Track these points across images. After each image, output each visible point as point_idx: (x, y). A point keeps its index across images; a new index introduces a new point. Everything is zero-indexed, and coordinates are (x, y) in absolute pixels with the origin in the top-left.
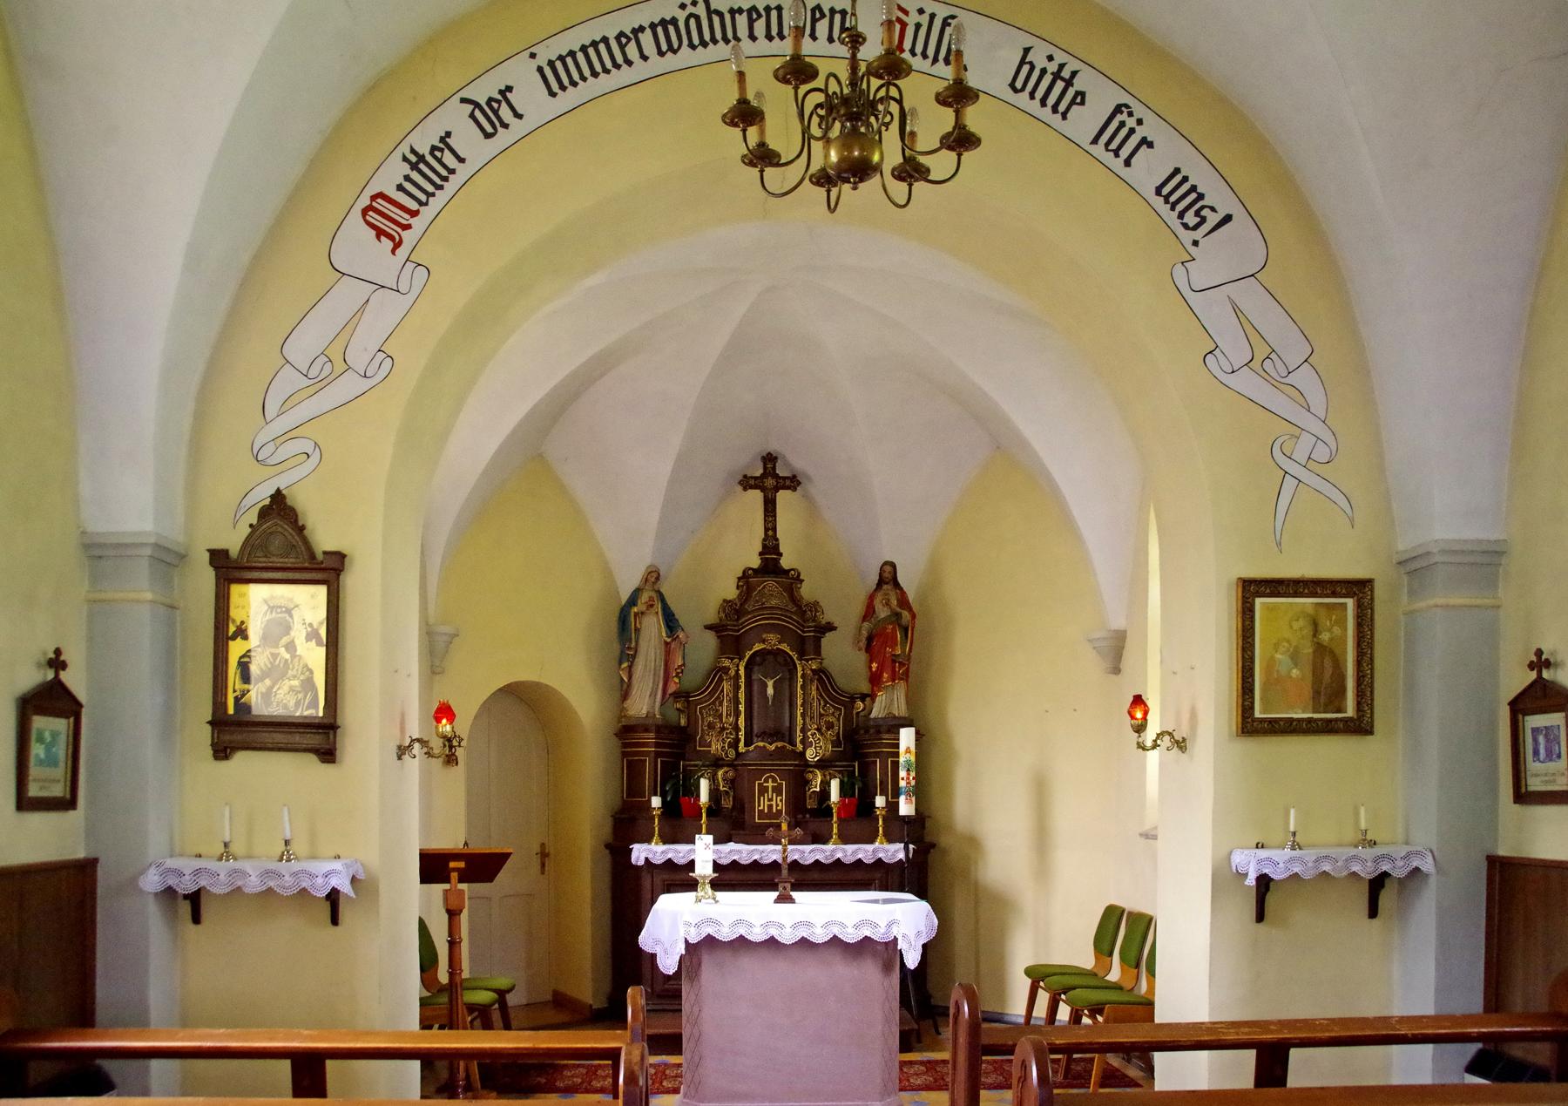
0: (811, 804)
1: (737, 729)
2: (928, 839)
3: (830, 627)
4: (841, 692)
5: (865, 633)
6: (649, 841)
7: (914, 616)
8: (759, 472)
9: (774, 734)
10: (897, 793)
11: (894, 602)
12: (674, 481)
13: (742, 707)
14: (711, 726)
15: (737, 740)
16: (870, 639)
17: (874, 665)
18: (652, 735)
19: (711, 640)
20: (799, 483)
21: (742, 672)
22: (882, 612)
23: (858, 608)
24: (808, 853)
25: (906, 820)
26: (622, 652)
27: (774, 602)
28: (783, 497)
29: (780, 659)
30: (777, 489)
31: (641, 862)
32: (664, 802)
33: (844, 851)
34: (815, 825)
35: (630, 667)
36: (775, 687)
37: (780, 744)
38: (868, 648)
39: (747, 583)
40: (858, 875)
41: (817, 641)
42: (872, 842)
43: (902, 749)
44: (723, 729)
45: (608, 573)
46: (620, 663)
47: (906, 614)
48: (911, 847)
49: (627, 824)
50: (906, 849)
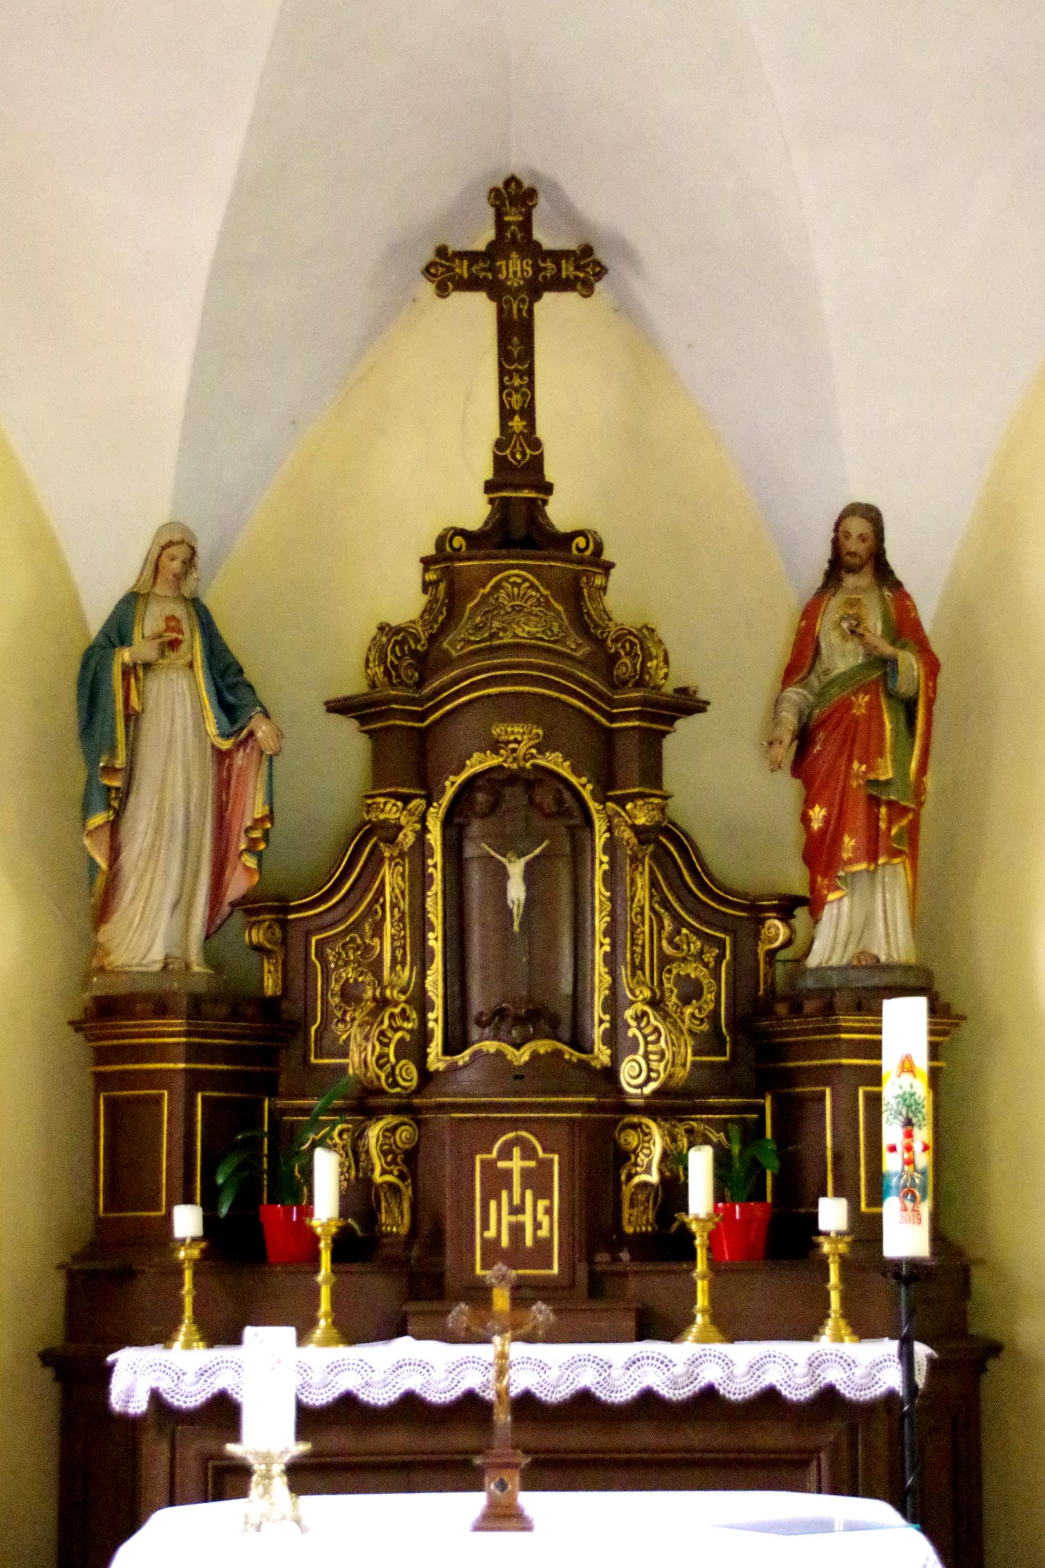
0: (636, 1220)
1: (423, 1004)
2: (976, 1328)
3: (687, 704)
4: (724, 894)
5: (790, 720)
6: (163, 1337)
7: (932, 666)
8: (482, 237)
9: (529, 1017)
10: (878, 1193)
11: (875, 624)
12: (230, 267)
13: (435, 941)
14: (349, 995)
15: (423, 1036)
16: (804, 737)
17: (818, 814)
18: (178, 1024)
19: (348, 745)
20: (601, 272)
21: (435, 837)
22: (841, 656)
23: (776, 645)
24: (621, 1369)
25: (910, 1273)
26: (90, 781)
27: (524, 631)
28: (554, 314)
29: (545, 798)
30: (535, 290)
31: (139, 1405)
32: (209, 1221)
33: (728, 1363)
34: (648, 1285)
35: (114, 827)
36: (530, 876)
37: (544, 1046)
38: (800, 766)
39: (449, 576)
40: (772, 1437)
41: (652, 744)
42: (808, 1332)
43: (889, 1062)
44: (382, 1003)
45: (43, 547)
46: (87, 810)
47: (909, 663)
48: (922, 1351)
49: (107, 1290)
50: (907, 1357)
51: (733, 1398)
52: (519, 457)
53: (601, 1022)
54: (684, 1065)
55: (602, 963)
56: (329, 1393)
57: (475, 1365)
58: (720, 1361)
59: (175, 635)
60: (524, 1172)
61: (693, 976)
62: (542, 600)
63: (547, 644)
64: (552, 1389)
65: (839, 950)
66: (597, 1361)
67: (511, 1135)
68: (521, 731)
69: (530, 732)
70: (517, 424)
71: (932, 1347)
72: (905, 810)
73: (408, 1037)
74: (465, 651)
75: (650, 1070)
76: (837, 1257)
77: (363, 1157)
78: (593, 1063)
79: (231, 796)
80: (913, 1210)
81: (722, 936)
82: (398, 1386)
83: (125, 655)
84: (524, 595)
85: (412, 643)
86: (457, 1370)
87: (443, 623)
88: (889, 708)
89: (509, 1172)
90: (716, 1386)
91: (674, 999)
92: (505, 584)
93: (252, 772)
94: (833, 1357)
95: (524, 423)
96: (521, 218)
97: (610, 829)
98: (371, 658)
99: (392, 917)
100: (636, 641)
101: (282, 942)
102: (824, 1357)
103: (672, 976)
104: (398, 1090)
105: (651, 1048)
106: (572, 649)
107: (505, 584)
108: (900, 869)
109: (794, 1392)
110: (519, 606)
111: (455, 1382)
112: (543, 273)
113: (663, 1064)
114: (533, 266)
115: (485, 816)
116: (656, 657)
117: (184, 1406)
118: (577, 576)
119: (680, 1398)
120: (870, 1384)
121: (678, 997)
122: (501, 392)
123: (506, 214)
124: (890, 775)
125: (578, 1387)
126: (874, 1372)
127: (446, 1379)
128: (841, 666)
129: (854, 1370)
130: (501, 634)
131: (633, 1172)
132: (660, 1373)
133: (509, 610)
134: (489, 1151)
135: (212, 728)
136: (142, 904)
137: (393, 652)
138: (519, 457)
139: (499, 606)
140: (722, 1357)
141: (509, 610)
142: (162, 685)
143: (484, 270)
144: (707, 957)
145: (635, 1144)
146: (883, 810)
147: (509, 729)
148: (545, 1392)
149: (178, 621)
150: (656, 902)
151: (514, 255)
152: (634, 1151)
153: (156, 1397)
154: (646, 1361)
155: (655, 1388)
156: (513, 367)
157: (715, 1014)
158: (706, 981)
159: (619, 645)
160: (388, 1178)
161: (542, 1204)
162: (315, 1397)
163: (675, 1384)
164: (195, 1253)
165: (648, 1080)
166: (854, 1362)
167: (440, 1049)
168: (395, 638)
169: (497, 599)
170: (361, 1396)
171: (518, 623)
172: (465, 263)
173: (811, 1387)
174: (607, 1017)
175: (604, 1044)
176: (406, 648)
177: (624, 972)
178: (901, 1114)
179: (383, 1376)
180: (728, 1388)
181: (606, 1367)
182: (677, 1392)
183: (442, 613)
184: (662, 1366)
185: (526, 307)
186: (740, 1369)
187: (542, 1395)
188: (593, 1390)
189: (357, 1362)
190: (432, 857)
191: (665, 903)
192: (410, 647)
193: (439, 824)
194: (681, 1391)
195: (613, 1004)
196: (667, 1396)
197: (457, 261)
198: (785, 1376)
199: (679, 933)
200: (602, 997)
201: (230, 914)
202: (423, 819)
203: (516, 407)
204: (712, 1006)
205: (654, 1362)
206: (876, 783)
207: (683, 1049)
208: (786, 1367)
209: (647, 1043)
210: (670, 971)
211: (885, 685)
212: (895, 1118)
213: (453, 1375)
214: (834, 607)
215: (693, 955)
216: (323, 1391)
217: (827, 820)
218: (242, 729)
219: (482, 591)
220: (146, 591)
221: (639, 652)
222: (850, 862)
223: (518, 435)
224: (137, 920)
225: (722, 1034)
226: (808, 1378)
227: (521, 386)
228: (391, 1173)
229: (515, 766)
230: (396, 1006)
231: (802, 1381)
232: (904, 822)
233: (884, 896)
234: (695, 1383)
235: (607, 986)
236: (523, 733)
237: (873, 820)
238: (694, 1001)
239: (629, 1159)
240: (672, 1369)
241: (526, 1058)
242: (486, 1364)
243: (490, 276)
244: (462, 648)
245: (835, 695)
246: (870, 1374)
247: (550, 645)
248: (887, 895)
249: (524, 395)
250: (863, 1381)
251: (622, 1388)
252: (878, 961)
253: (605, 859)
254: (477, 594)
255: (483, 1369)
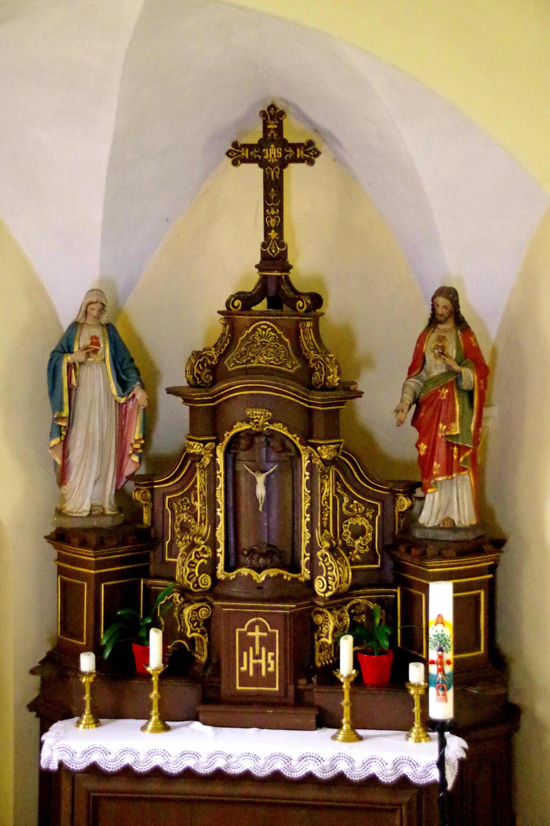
1: (214, 545)
11: (452, 351)
12: (116, 167)
13: (220, 513)
15: (214, 560)
20: (318, 153)
21: (220, 460)
22: (435, 367)
28: (295, 175)
31: (54, 766)
32: (99, 663)
36: (267, 484)
45: (36, 290)
47: (469, 376)
51: (354, 779)
52: (274, 251)
53: (305, 557)
54: (347, 582)
55: (306, 527)
56: (148, 766)
57: (222, 755)
58: (347, 760)
59: (95, 347)
60: (261, 638)
61: (360, 524)
62: (277, 337)
63: (275, 367)
64: (261, 770)
65: (433, 518)
66: (284, 756)
67: (254, 619)
68: (260, 413)
69: (265, 414)
70: (273, 234)
71: (469, 745)
72: (468, 449)
73: (206, 562)
74: (234, 368)
75: (328, 585)
76: (418, 696)
77: (182, 622)
78: (300, 579)
79: (126, 424)
80: (443, 695)
81: (377, 503)
82: (183, 764)
83: (68, 359)
84: (268, 335)
85: (209, 361)
86: (213, 757)
87: (227, 347)
88: (459, 396)
89: (254, 638)
90: (345, 773)
91: (349, 537)
92: (258, 329)
93: (135, 415)
94: (406, 761)
95: (277, 234)
96: (276, 127)
97: (310, 459)
98: (188, 370)
99: (200, 498)
100: (323, 365)
101: (151, 500)
102: (402, 761)
103: (348, 526)
104: (200, 590)
105: (329, 573)
106: (289, 368)
107: (258, 329)
108: (467, 477)
109: (385, 778)
110: (264, 342)
111: (212, 763)
112: (287, 156)
113: (334, 583)
114: (282, 153)
115: (245, 450)
116: (332, 373)
117: (76, 769)
118: (298, 322)
119: (327, 778)
120: (426, 776)
121: (351, 536)
122: (265, 217)
123: (268, 124)
124: (458, 432)
125: (275, 769)
126: (428, 769)
127: (207, 762)
128: (435, 372)
129: (417, 768)
130: (252, 361)
131: (320, 636)
132: (316, 765)
133: (259, 344)
134: (243, 627)
135: (114, 392)
136: (79, 481)
137: (198, 367)
138: (274, 251)
139: (254, 342)
140: (349, 758)
141: (259, 344)
142: (89, 370)
143: (257, 154)
144: (368, 514)
145: (321, 622)
146: (455, 449)
147: (254, 412)
148: (257, 771)
149: (97, 338)
150: (339, 489)
151: (272, 146)
152: (321, 625)
153: (61, 764)
154: (309, 758)
155: (314, 772)
156: (271, 205)
157: (372, 545)
158: (368, 527)
159: (315, 364)
160: (194, 634)
161: (270, 654)
162: (141, 767)
163: (324, 770)
164: (91, 679)
165: (328, 590)
166: (417, 764)
167: (222, 567)
168: (199, 360)
169: (254, 338)
170: (164, 768)
171: (261, 355)
172: (247, 150)
173: (395, 775)
174: (308, 554)
175: (306, 568)
176: (205, 365)
177: (318, 533)
178: (436, 645)
179: (175, 759)
180: (351, 774)
181: (289, 760)
182: (325, 774)
183: (226, 342)
184: (318, 761)
185: (278, 173)
186: (357, 765)
187: (256, 773)
188: (282, 771)
189: (162, 751)
190: (219, 470)
191: (345, 489)
192: (207, 363)
193: (222, 454)
194: (327, 774)
195: (312, 548)
196: (320, 776)
197: (243, 149)
198: (381, 769)
199: (352, 503)
200: (306, 544)
201: (127, 482)
202: (214, 452)
203: (273, 226)
204: (371, 539)
205: (313, 759)
206: (451, 436)
207: (346, 574)
208: (382, 765)
209: (327, 570)
210: (347, 523)
211: (457, 383)
212: (434, 647)
213: (211, 760)
214: (432, 337)
215: (360, 514)
216: (145, 764)
217: (427, 450)
218: (129, 393)
219: (247, 331)
220: (82, 322)
221: (323, 371)
222: (438, 476)
223: (273, 240)
224: (77, 489)
225: (376, 553)
226: (393, 771)
227: (275, 214)
228: (196, 632)
229: (258, 430)
230: (199, 547)
231: (390, 772)
232: (468, 454)
233: (457, 492)
234: (335, 770)
235: (308, 538)
236: (262, 415)
237: (449, 453)
238: (361, 537)
239: (318, 628)
240: (323, 763)
241: (263, 579)
242: (227, 755)
243: (260, 157)
244: (233, 366)
245: (431, 388)
246: (425, 771)
247: (277, 367)
248: (459, 490)
249: (277, 219)
250: (421, 774)
251: (297, 770)
252: (454, 524)
253: (307, 474)
254: (245, 332)
255: (226, 757)
